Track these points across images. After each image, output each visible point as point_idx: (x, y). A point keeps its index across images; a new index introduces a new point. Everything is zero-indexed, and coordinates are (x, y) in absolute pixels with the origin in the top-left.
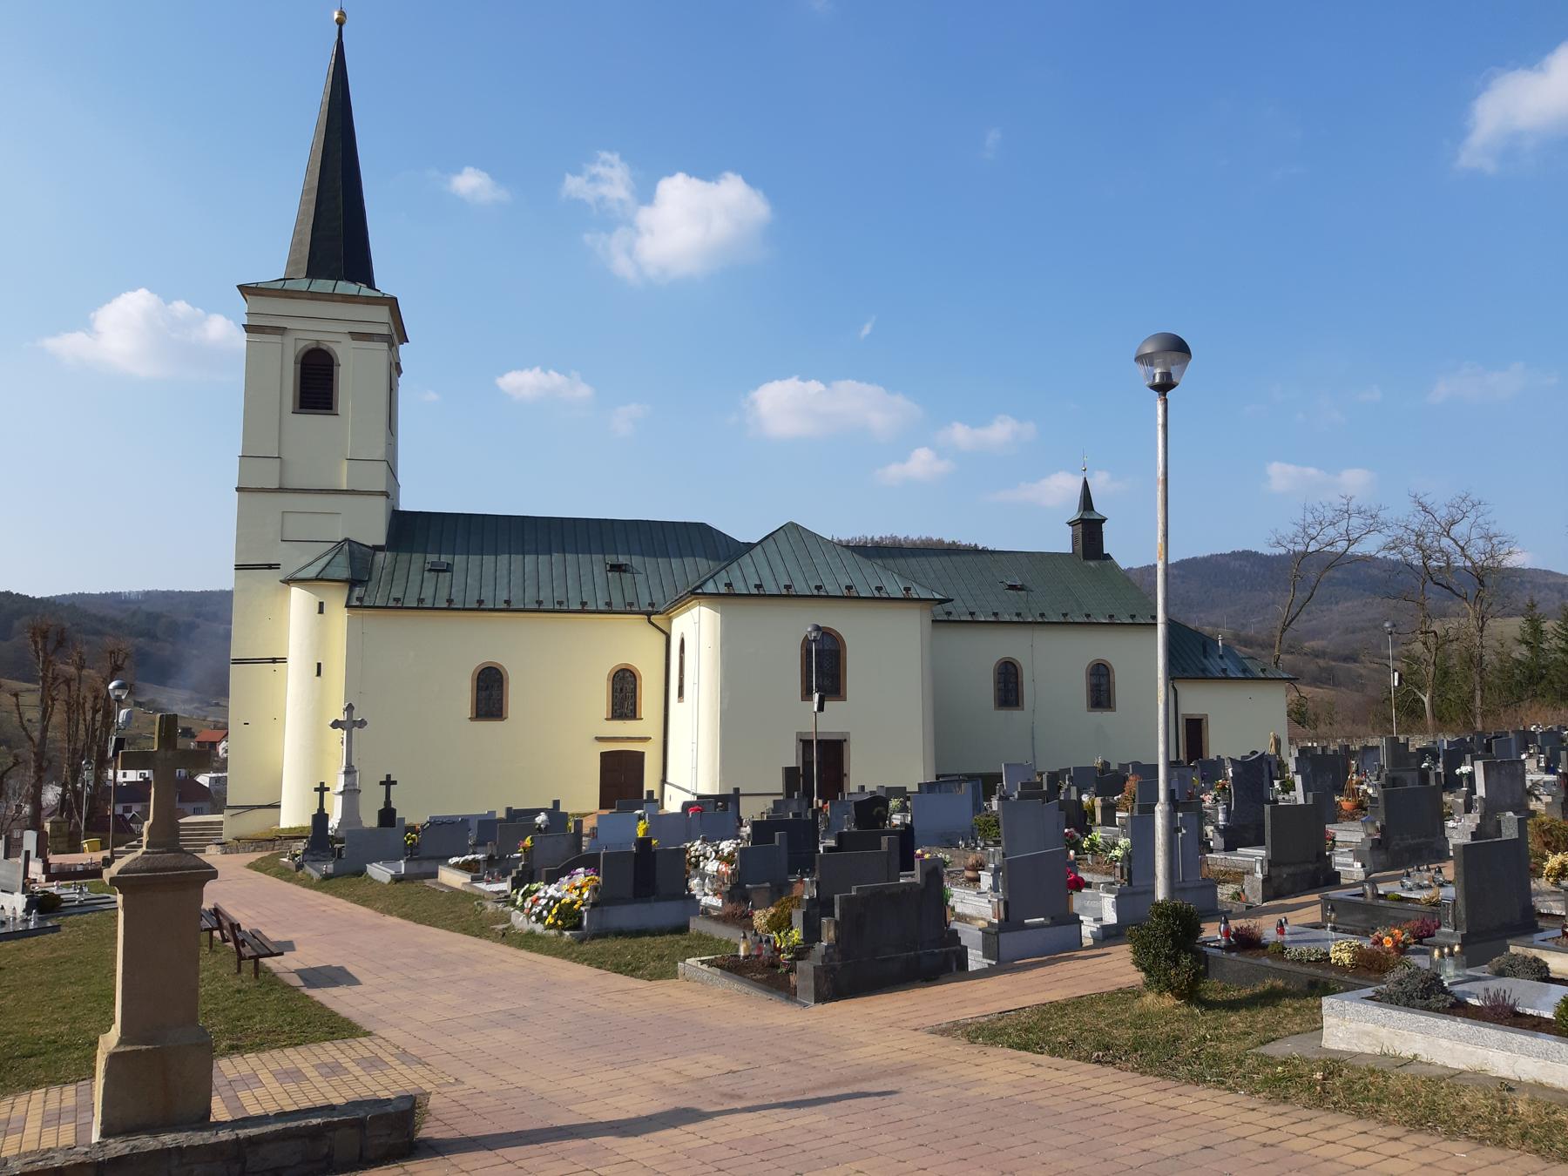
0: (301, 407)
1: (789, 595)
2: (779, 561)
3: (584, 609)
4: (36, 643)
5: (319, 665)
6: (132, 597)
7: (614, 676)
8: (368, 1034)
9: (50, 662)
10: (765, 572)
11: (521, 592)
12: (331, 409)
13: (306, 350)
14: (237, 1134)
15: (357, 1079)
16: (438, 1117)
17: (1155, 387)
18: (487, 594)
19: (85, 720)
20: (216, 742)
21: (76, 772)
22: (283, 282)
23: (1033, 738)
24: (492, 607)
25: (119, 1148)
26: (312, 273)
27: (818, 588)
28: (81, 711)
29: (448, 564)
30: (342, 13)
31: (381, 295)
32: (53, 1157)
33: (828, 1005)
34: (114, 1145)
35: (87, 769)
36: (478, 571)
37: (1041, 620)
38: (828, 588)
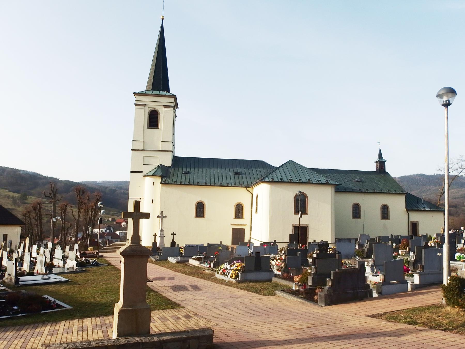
0: (149, 127)
1: (290, 182)
2: (287, 172)
3: (227, 186)
4: (77, 193)
5: (153, 200)
6: (100, 182)
7: (236, 206)
8: (183, 307)
9: (81, 198)
10: (283, 175)
11: (209, 180)
12: (157, 127)
13: (151, 110)
14: (159, 339)
15: (185, 322)
16: (217, 336)
17: (443, 105)
18: (200, 180)
19: (89, 214)
20: (121, 223)
21: (87, 229)
22: (145, 92)
23: (364, 228)
24: (201, 184)
25: (123, 341)
26: (153, 89)
27: (300, 180)
28: (88, 212)
29: (189, 172)
30: (163, 16)
31: (172, 95)
32: (104, 342)
33: (329, 307)
34: (121, 340)
35: (90, 228)
36: (197, 174)
37: (367, 191)
38: (303, 180)
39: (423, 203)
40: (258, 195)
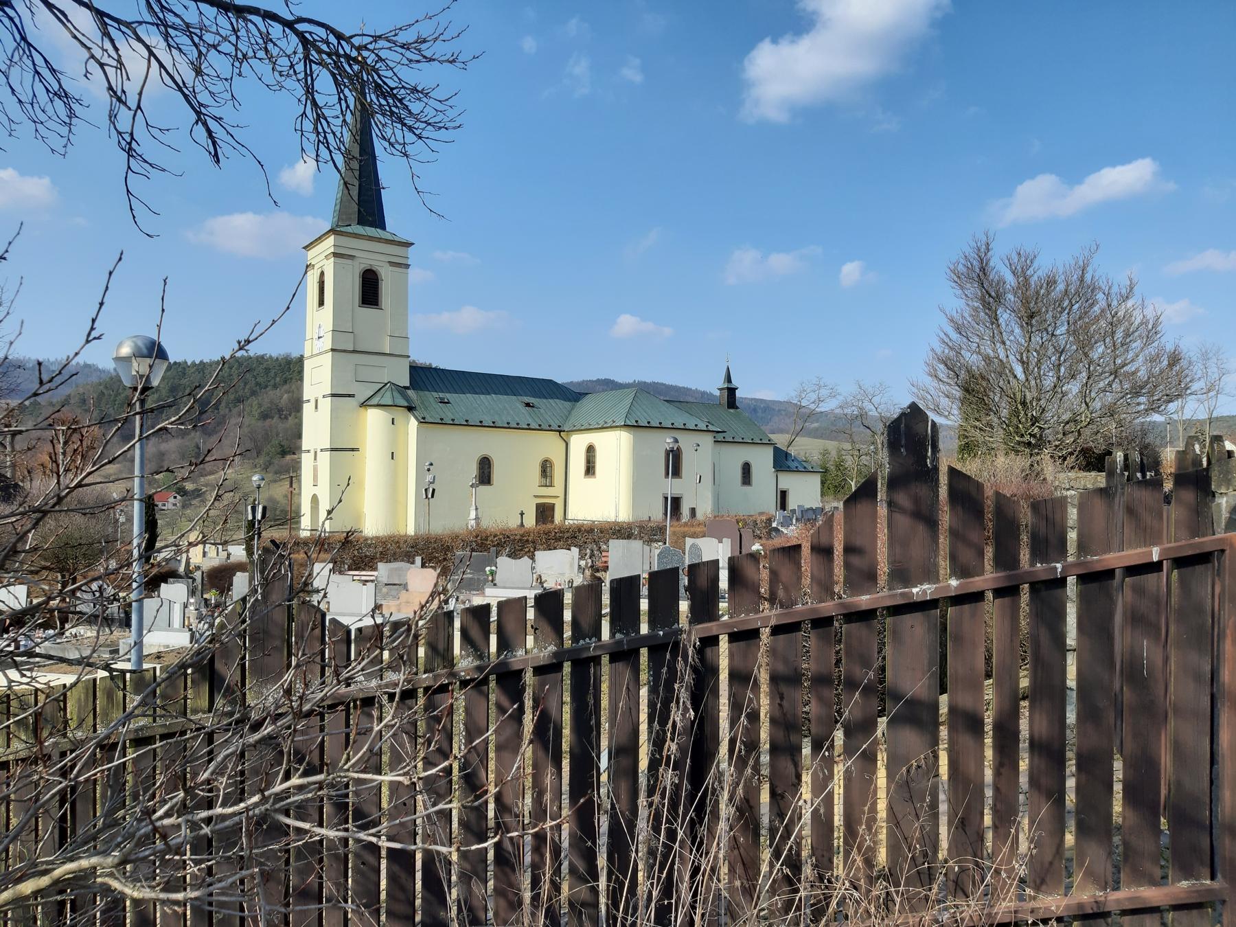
39: (462, 849)
40: (209, 160)
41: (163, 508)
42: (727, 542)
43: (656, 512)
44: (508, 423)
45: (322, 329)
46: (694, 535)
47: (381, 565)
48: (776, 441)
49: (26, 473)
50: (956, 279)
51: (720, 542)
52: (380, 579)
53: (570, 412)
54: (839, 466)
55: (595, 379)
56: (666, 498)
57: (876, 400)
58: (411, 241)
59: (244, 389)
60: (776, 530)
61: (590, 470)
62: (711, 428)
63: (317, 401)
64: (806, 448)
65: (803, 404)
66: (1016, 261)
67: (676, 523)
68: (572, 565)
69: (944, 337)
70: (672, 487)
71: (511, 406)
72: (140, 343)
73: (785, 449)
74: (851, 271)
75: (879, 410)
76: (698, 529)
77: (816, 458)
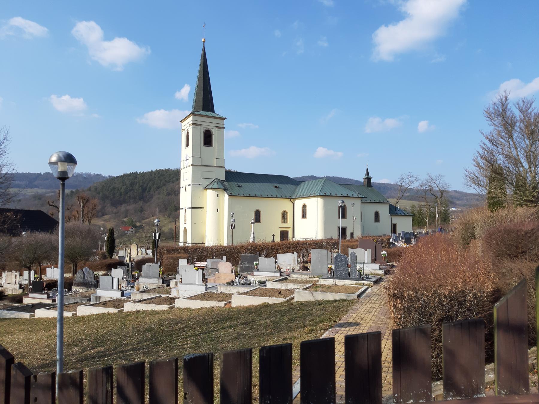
5: (218, 209)
30: (205, 40)
41: (127, 233)
42: (369, 251)
43: (335, 235)
44: (268, 195)
45: (188, 156)
46: (353, 247)
47: (208, 260)
48: (391, 202)
49: (68, 219)
50: (489, 116)
51: (366, 250)
52: (208, 266)
53: (295, 190)
54: (420, 213)
55: (307, 176)
56: (339, 228)
57: (437, 182)
58: (225, 117)
59: (160, 183)
60: (392, 243)
61: (304, 216)
62: (360, 196)
63: (186, 187)
64: (404, 204)
65: (402, 185)
66: (522, 104)
67: (344, 241)
68: (294, 260)
69: (484, 146)
70: (342, 223)
71: (269, 187)
72: (61, 155)
73: (395, 205)
74: (423, 125)
75: (439, 187)
76: (355, 244)
77: (409, 208)
